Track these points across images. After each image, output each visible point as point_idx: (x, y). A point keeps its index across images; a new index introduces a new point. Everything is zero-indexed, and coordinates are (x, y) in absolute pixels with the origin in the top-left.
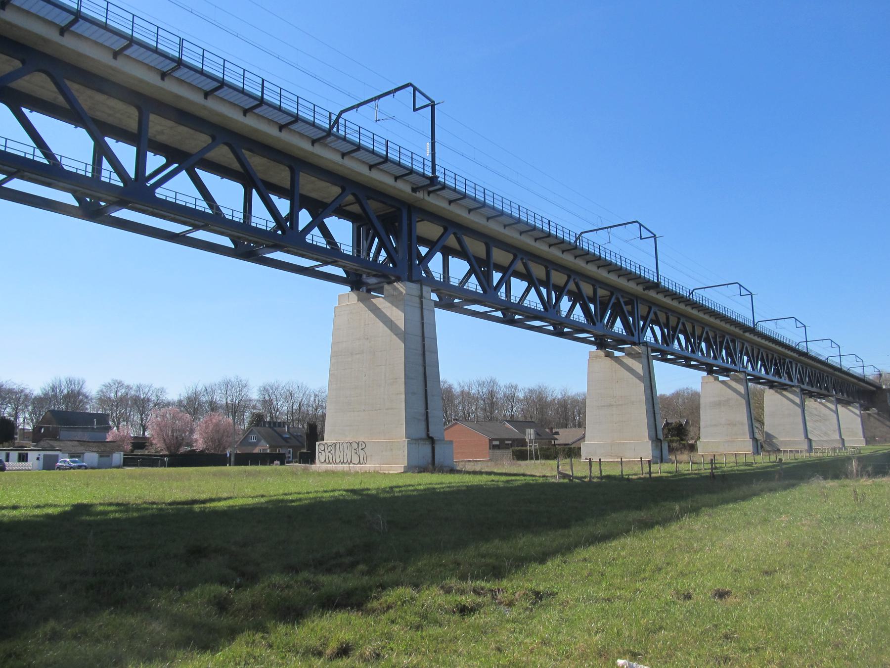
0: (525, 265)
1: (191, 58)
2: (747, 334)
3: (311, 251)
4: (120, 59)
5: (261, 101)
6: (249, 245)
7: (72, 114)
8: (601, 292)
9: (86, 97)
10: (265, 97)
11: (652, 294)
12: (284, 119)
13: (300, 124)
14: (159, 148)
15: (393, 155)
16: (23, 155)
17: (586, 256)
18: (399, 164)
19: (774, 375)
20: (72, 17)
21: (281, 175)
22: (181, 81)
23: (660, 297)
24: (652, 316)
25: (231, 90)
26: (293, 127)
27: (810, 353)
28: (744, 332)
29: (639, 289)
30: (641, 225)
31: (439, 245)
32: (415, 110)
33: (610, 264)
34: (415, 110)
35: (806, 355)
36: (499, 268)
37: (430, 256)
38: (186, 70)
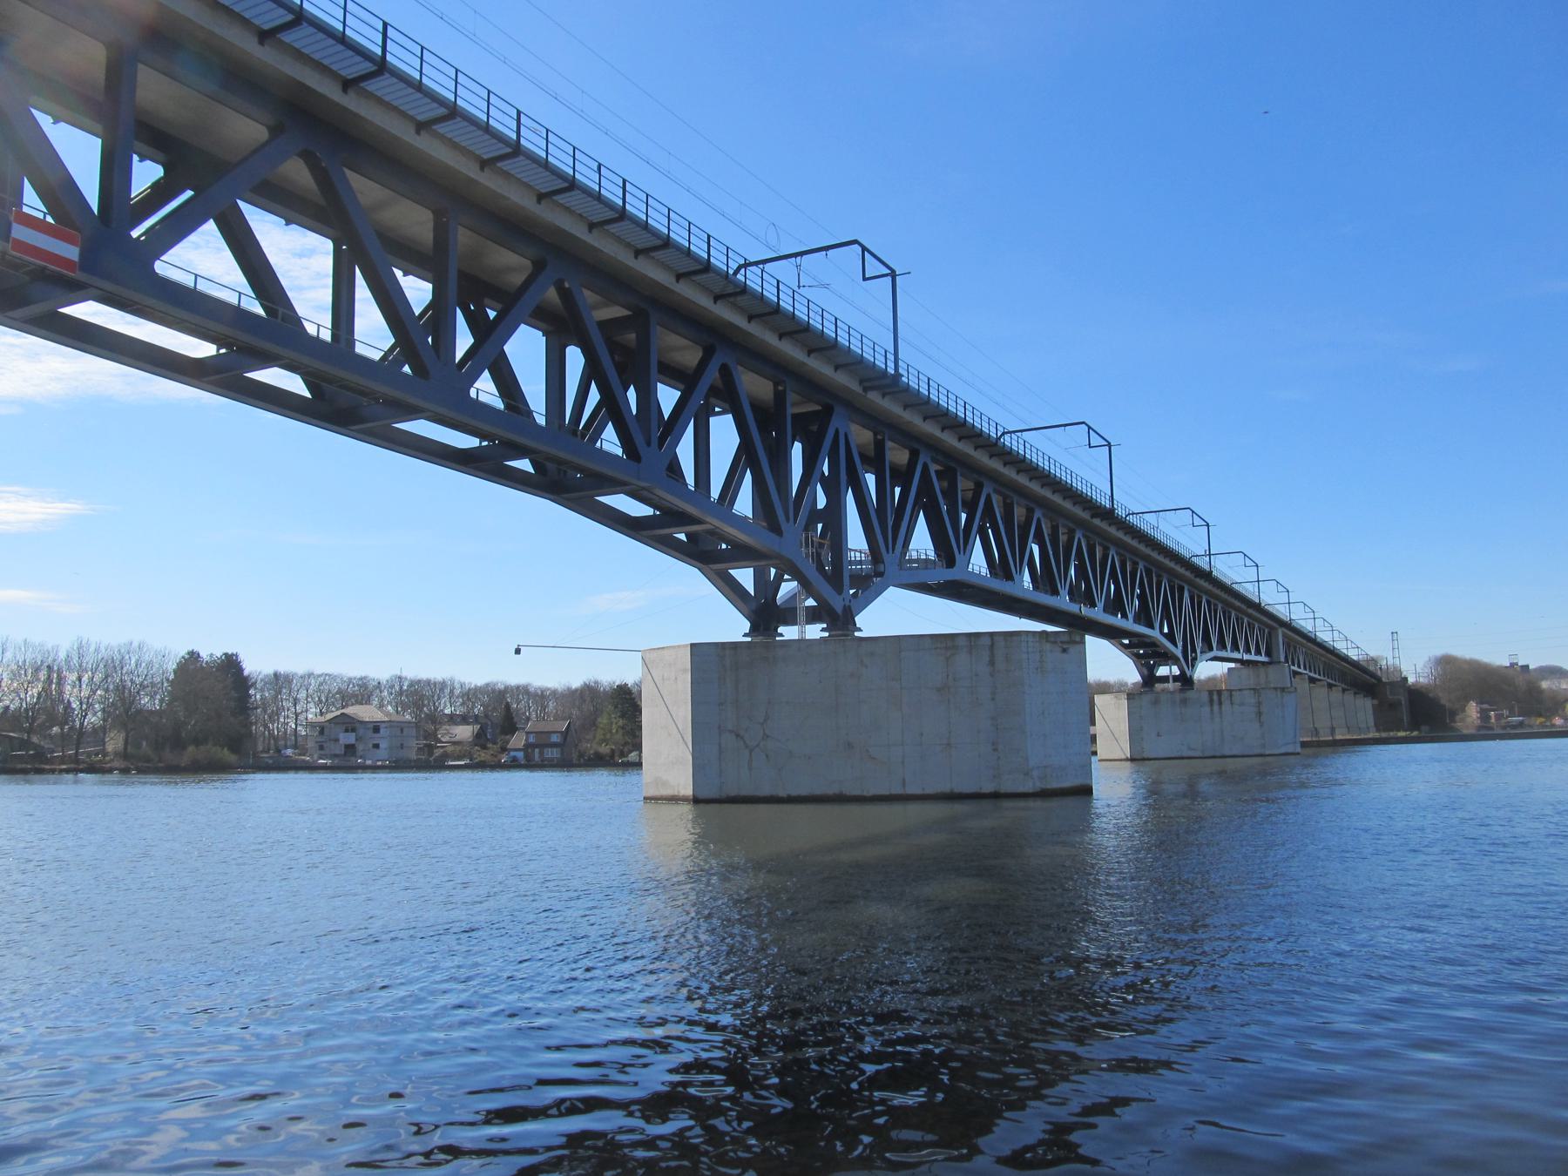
0: (565, 294)
1: (532, 142)
2: (1097, 521)
3: (466, 415)
4: (351, 93)
5: (516, 149)
6: (346, 400)
7: (318, 210)
8: (897, 455)
9: (364, 188)
10: (523, 141)
11: (1202, 582)
12: (427, 111)
13: (625, 224)
14: (159, 141)
15: (635, 207)
16: (188, 281)
17: (770, 313)
18: (645, 226)
19: (1137, 620)
20: (290, 17)
21: (415, 220)
22: (300, 56)
23: (1112, 530)
24: (712, 376)
25: (321, 36)
26: (441, 128)
27: (1120, 512)
28: (1093, 516)
29: (1085, 515)
30: (864, 249)
31: (528, 302)
32: (865, 279)
33: (946, 413)
34: (865, 279)
35: (1207, 575)
36: (673, 375)
37: (114, 171)
38: (312, 30)
